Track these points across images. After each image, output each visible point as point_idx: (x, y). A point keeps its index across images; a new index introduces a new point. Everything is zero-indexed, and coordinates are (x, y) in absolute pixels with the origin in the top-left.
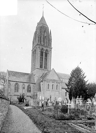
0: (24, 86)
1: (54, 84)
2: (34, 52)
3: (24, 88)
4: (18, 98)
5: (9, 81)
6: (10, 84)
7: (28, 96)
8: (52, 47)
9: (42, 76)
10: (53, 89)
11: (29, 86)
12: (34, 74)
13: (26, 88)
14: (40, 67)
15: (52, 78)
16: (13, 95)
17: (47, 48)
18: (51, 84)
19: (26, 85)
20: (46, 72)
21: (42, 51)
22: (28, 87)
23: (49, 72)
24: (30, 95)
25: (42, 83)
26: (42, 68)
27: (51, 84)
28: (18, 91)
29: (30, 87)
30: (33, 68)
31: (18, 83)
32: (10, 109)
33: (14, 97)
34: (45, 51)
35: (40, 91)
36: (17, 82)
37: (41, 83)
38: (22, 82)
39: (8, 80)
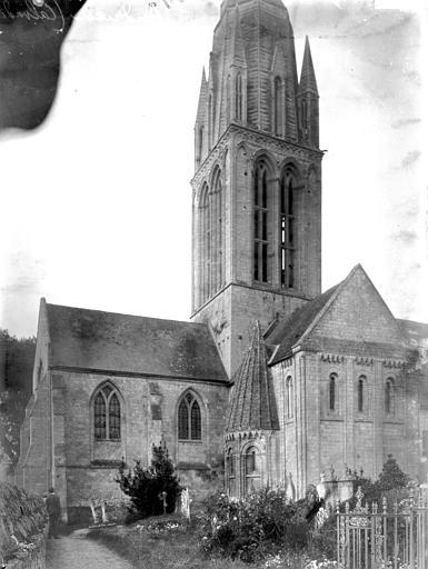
0: (154, 400)
1: (367, 371)
2: (209, 193)
3: (157, 413)
4: (125, 483)
5: (56, 372)
6: (64, 390)
7: (186, 467)
8: (321, 148)
9: (272, 329)
10: (360, 409)
11: (190, 397)
12: (215, 322)
13: (170, 413)
14: (256, 277)
15: (350, 334)
16: (85, 462)
17: (290, 154)
18: (348, 373)
19: (173, 390)
20: (295, 303)
21: (261, 172)
22: (182, 407)
23: (320, 303)
24: (197, 460)
25: (289, 371)
26: (265, 280)
27: (348, 373)
28: (116, 436)
29: (196, 407)
30: (207, 288)
31: (113, 378)
32: (18, 351)
33: (93, 474)
34: (278, 175)
35: (274, 425)
36: (106, 373)
37: (276, 370)
38: (147, 376)
39: (45, 366)
